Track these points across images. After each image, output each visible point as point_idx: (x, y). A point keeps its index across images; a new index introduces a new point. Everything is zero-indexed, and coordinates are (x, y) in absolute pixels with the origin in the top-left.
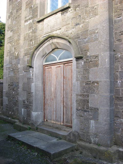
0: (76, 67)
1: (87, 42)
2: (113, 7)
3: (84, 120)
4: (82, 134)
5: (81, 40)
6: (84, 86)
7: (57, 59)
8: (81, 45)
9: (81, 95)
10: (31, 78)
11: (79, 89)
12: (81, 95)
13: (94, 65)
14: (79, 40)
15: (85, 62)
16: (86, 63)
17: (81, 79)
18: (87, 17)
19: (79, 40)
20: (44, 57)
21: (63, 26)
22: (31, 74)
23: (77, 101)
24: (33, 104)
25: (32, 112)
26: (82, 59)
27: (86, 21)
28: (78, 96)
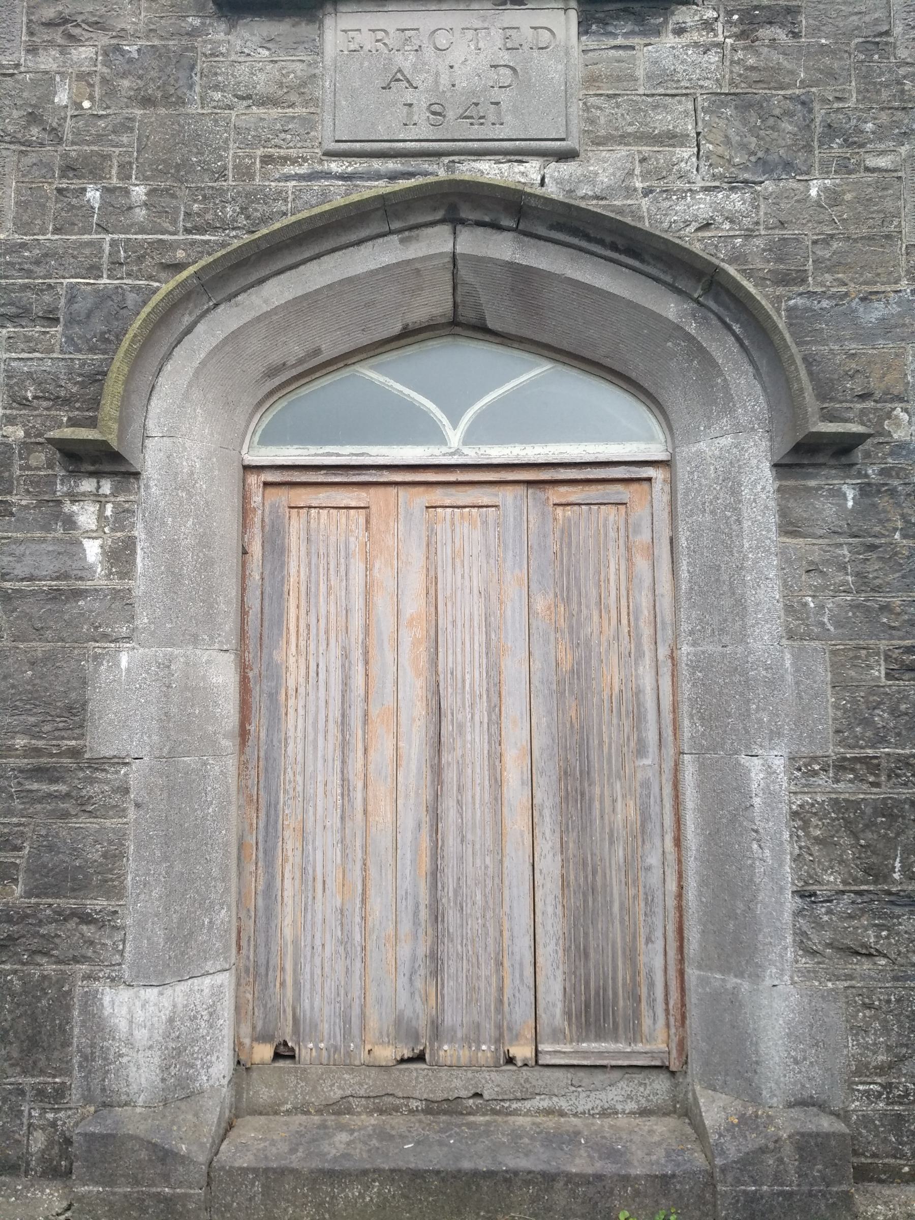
0: (773, 520)
1: (886, 327)
2: (288, 184)
3: (896, 979)
4: (884, 1115)
5: (825, 304)
6: (874, 689)
7: (454, 437)
8: (815, 342)
9: (842, 766)
10: (78, 594)
11: (826, 711)
12: (842, 766)
13: (34, 915)
14: (799, 301)
15: (865, 490)
16: (883, 502)
17: (838, 624)
18: (881, 134)
19: (799, 301)
20: (277, 381)
21: (599, 142)
22: (93, 550)
23: (800, 817)
24: (113, 890)
25: (91, 1000)
26: (844, 460)
27: (872, 162)
28: (815, 773)
